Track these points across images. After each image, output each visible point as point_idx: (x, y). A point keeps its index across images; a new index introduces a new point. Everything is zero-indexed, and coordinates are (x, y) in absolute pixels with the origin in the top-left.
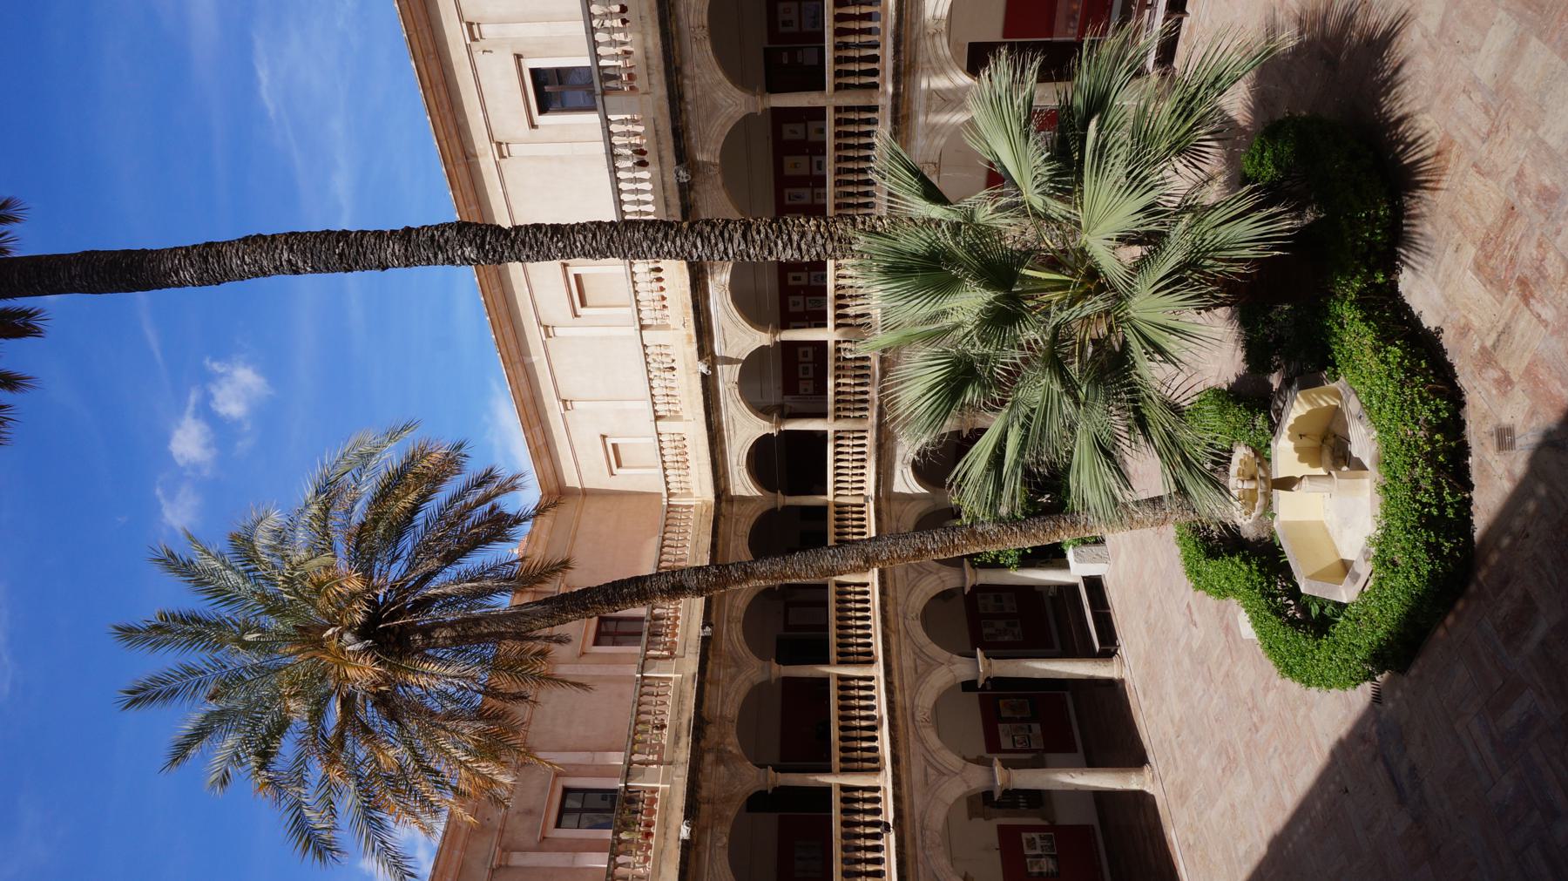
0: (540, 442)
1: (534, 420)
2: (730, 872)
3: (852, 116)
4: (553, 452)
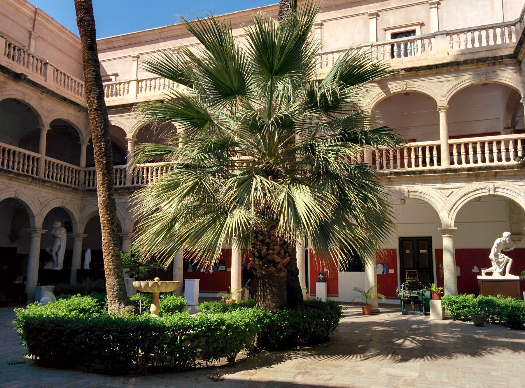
0: (116, 44)
1: (128, 42)
2: (7, 97)
3: (92, 177)
4: (108, 50)
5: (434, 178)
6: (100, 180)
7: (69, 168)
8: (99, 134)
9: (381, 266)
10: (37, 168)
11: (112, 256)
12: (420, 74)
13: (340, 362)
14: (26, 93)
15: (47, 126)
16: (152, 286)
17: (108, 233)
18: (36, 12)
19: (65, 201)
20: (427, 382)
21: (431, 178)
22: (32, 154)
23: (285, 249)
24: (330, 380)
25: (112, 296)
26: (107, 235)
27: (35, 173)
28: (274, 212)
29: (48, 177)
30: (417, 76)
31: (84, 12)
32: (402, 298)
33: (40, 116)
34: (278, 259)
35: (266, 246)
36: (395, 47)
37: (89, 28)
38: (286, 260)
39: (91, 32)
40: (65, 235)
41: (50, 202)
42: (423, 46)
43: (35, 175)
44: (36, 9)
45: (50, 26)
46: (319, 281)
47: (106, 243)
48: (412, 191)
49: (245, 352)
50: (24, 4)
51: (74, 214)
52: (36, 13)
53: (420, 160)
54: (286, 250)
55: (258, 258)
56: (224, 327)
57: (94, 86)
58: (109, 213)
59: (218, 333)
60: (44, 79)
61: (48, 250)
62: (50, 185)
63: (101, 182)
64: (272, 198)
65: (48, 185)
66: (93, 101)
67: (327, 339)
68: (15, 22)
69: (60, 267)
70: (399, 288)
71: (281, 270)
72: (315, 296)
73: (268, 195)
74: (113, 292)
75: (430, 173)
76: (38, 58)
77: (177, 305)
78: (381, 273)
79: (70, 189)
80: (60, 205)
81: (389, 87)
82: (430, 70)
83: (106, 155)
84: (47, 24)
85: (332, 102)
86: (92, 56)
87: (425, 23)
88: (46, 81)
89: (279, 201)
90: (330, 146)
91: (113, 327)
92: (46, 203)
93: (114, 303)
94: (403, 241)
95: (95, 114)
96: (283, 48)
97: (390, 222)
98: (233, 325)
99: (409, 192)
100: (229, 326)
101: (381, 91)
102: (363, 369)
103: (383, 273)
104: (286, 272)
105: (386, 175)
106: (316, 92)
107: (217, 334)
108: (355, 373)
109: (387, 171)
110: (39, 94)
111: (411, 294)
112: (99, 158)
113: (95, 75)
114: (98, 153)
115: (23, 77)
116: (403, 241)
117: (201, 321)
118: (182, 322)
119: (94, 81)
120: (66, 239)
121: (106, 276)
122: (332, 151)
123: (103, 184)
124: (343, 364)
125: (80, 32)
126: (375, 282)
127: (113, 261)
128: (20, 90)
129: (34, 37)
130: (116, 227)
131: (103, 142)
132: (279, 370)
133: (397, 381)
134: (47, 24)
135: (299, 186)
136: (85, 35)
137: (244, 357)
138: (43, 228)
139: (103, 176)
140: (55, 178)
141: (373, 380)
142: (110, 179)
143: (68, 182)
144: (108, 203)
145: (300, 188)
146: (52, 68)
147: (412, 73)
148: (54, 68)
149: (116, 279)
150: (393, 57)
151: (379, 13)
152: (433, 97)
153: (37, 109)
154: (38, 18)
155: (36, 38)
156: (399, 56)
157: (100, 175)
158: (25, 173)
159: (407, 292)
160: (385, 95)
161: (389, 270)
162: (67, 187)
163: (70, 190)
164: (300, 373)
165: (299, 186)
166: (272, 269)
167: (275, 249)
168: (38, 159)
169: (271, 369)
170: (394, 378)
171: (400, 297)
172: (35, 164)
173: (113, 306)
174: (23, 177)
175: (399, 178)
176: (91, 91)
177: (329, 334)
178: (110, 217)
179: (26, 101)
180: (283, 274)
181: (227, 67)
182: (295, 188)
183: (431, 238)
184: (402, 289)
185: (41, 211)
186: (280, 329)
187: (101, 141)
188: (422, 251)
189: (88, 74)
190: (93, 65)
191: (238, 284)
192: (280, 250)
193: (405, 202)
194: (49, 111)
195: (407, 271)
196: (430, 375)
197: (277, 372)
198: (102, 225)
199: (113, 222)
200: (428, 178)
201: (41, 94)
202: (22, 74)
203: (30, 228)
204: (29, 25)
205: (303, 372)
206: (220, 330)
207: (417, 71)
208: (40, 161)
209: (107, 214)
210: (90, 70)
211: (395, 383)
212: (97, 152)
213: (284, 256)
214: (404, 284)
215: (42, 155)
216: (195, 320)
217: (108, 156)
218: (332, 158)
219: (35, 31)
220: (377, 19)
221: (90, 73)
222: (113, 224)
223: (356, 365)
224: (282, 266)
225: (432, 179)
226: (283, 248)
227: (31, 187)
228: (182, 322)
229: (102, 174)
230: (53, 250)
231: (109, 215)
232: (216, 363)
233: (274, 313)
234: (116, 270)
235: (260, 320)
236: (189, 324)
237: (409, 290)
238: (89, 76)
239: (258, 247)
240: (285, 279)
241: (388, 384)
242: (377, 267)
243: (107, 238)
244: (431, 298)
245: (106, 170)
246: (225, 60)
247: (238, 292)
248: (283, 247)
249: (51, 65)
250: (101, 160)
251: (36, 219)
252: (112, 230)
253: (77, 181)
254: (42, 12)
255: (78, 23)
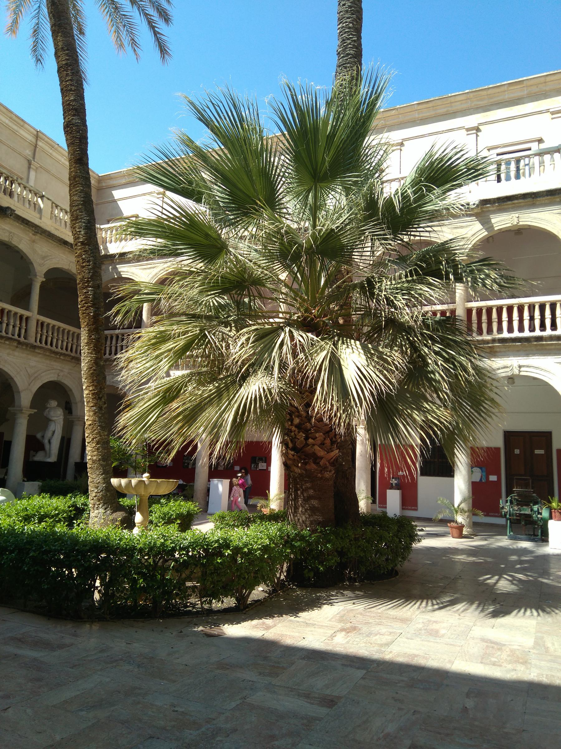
5: (557, 347)
6: (84, 339)
7: (69, 332)
8: (86, 276)
9: (479, 470)
10: (26, 330)
11: (98, 443)
12: (538, 203)
13: (409, 613)
14: (14, 233)
15: (40, 277)
16: (135, 486)
17: (93, 411)
18: (38, 135)
19: (61, 374)
20: (549, 658)
21: (553, 347)
22: (20, 311)
23: (332, 438)
24: (388, 644)
25: (95, 498)
26: (91, 414)
27: (22, 336)
28: (308, 377)
29: (41, 341)
30: (533, 206)
31: (72, 114)
32: (508, 516)
33: (32, 264)
34: (321, 453)
35: (304, 434)
36: (503, 167)
37: (78, 134)
38: (332, 454)
39: (80, 141)
40: (62, 417)
41: (42, 375)
42: (542, 163)
43: (22, 339)
44: (38, 132)
45: (54, 154)
46: (392, 487)
47: (90, 425)
48: (524, 366)
49: (266, 588)
50: (22, 126)
51: (73, 391)
52: (37, 137)
53: (537, 323)
54: (334, 439)
55: (292, 449)
56: (229, 551)
57: (81, 212)
58: (96, 384)
59: (219, 561)
60: (38, 216)
61: (39, 436)
62: (42, 352)
63: (86, 341)
64: (305, 358)
65: (39, 352)
66: (80, 232)
67: (393, 573)
68: (9, 147)
69: (53, 458)
70: (504, 501)
71: (325, 468)
72: (386, 507)
73: (301, 356)
74: (96, 492)
75: (551, 341)
76: (31, 188)
77: (182, 514)
78: (478, 480)
79: (68, 358)
80: (56, 379)
81: (493, 221)
82: (553, 197)
83: (93, 305)
84: (51, 151)
85: (401, 210)
86: (80, 172)
87: (544, 139)
88: (41, 218)
89: (316, 364)
90: (399, 283)
91: (55, 546)
92: (36, 375)
93: (97, 509)
94: (509, 436)
95: (81, 249)
96: (331, 137)
97: (492, 400)
98: (244, 548)
99: (520, 367)
100: (237, 550)
101: (481, 227)
102: (444, 628)
103: (481, 480)
104: (333, 472)
105: (487, 342)
106: (378, 196)
107: (217, 562)
108: (430, 634)
109: (489, 338)
110: (31, 234)
111: (521, 511)
112: (84, 308)
113: (83, 197)
114: (84, 302)
115: (10, 212)
116: (509, 436)
117: (192, 541)
118: (163, 541)
119: (82, 205)
120: (62, 423)
121: (88, 470)
122: (402, 290)
123: (88, 344)
124: (414, 616)
125: (67, 140)
126: (469, 492)
127: (98, 449)
128: (6, 228)
129: (35, 168)
130: (105, 403)
131: (90, 287)
132: (311, 622)
133: (499, 653)
134: (51, 151)
135: (350, 341)
136: (73, 144)
137: (262, 596)
138: (32, 406)
139: (89, 333)
140: (49, 343)
141: (458, 648)
142: (99, 338)
143: (67, 349)
144: (94, 370)
145: (347, 342)
146: (50, 203)
147: (526, 200)
148: (53, 203)
149: (102, 474)
150: (499, 180)
151: (480, 127)
152: (557, 234)
153: (28, 255)
154: (40, 143)
155: (37, 168)
156: (508, 179)
157: (85, 332)
158: (10, 336)
159: (516, 508)
160: (486, 233)
161: (496, 480)
162: (64, 355)
163: (70, 360)
164: (342, 630)
165: (346, 340)
166: (312, 466)
167: (317, 438)
168: (27, 319)
169: (297, 619)
170: (493, 647)
171: (505, 515)
172: (24, 324)
173: (96, 511)
174: (5, 340)
175: (505, 347)
176: (77, 219)
177: (396, 565)
178: (97, 389)
179: (13, 243)
180: (327, 475)
181: (247, 165)
182: (345, 346)
183: (550, 434)
184: (508, 504)
185: (29, 385)
186: (320, 557)
187: (88, 286)
188: (537, 452)
189: (74, 195)
190: (82, 184)
191: (280, 488)
192: (325, 439)
193: (514, 383)
194: (43, 258)
195: (516, 479)
196: (553, 644)
197: (307, 625)
198: (85, 400)
199: (101, 396)
200: (548, 347)
201: (33, 234)
202: (8, 208)
203: (14, 406)
204: (28, 152)
205: (348, 629)
206: (222, 555)
207: (533, 198)
208: (29, 321)
209: (92, 385)
210: (77, 191)
211: (496, 655)
212: (82, 301)
213: (331, 449)
214: (511, 497)
215: (33, 314)
216: (185, 540)
217: (97, 306)
218: (403, 301)
219: (36, 160)
220: (477, 136)
221: (76, 194)
222: (100, 398)
223: (433, 619)
224: (327, 463)
225: (554, 349)
226: (329, 436)
227: (16, 353)
228: (163, 541)
229: (88, 330)
230: (45, 436)
231: (96, 386)
232: (216, 605)
233: (313, 531)
234: (103, 463)
235: (288, 541)
236: (172, 545)
237: (518, 505)
238: (75, 198)
239: (293, 434)
240: (331, 483)
241: (482, 658)
242: (472, 471)
243: (91, 419)
244: (551, 518)
245: (93, 325)
246: (243, 152)
247: (280, 499)
248: (329, 436)
249: (48, 199)
250: (87, 312)
251: (23, 395)
252: (99, 407)
253: (74, 347)
254: (45, 136)
255: (64, 128)
